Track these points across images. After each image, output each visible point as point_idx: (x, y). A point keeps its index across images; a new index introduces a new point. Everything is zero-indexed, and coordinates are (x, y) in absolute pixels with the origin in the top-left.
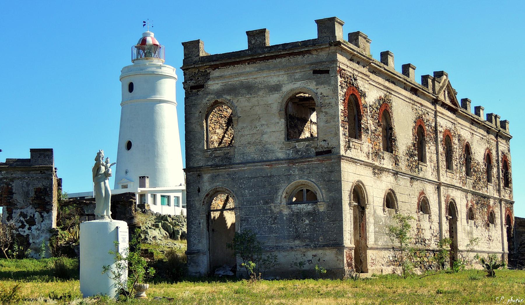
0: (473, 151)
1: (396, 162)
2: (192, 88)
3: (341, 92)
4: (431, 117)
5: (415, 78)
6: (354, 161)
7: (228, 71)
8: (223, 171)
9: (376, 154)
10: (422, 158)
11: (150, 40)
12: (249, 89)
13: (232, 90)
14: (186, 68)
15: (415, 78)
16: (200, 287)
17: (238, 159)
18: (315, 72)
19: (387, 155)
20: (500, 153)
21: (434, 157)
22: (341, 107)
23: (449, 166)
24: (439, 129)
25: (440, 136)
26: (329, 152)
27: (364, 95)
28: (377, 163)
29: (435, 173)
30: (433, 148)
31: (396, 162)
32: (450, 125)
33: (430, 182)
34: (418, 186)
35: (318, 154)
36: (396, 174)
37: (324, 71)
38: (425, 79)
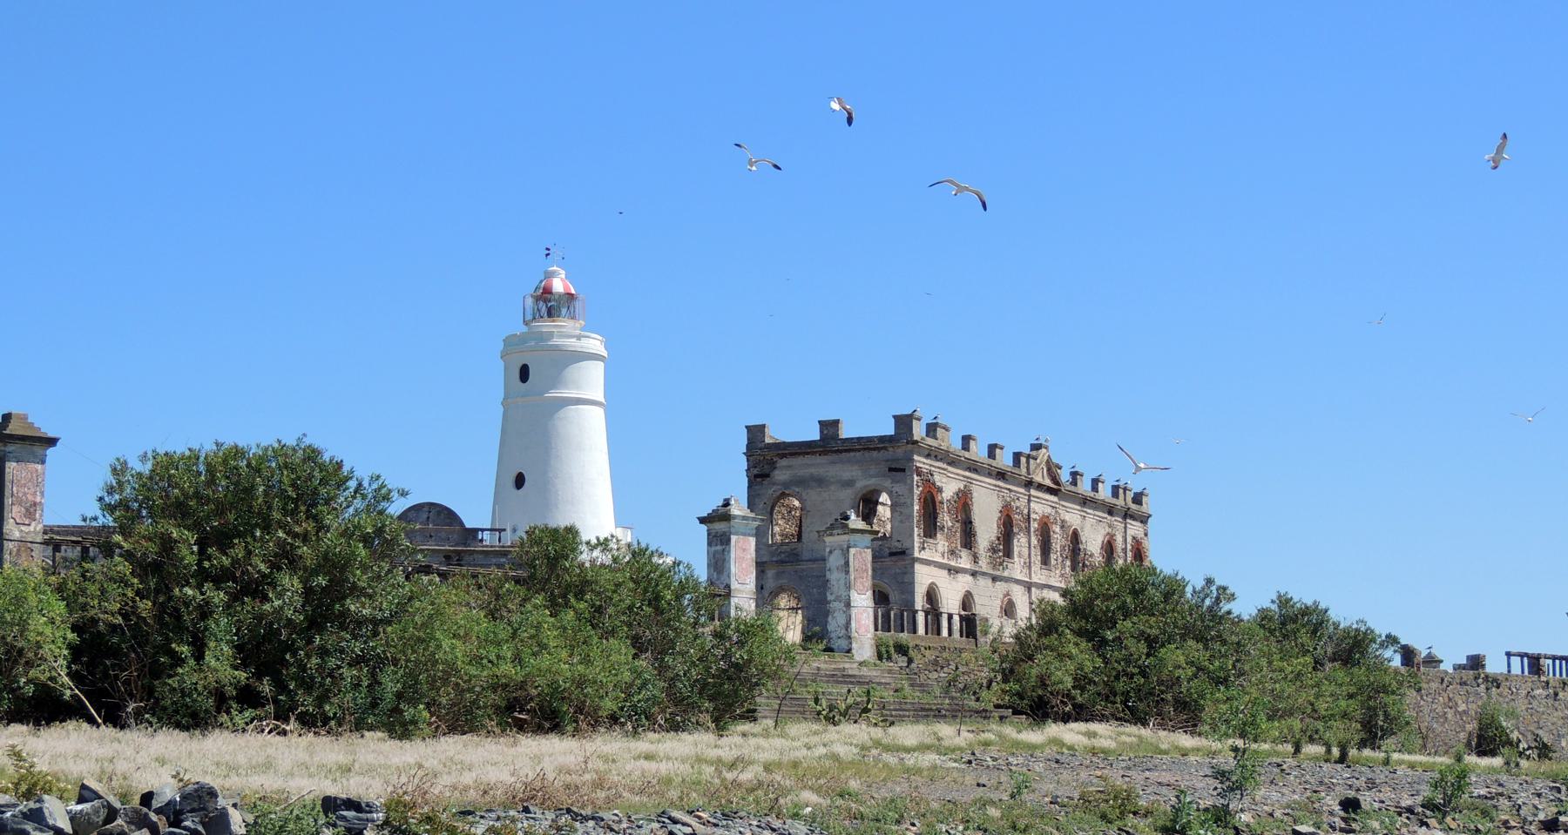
0: (1083, 539)
1: (975, 559)
2: (756, 476)
3: (917, 492)
4: (1024, 500)
5: (1004, 460)
6: (927, 562)
7: (799, 461)
8: (789, 568)
9: (952, 552)
10: (1008, 553)
11: (558, 286)
12: (820, 482)
13: (802, 482)
14: (750, 453)
15: (1004, 460)
16: (675, 744)
17: (806, 555)
18: (891, 470)
19: (964, 553)
20: (1129, 539)
21: (1025, 551)
22: (916, 508)
23: (1045, 561)
24: (1033, 516)
25: (1034, 525)
26: (903, 553)
27: (940, 490)
28: (953, 563)
29: (1026, 570)
30: (1024, 540)
31: (975, 559)
32: (1049, 510)
33: (1018, 582)
34: (1001, 586)
35: (892, 554)
36: (974, 574)
37: (899, 470)
38: (1017, 456)
